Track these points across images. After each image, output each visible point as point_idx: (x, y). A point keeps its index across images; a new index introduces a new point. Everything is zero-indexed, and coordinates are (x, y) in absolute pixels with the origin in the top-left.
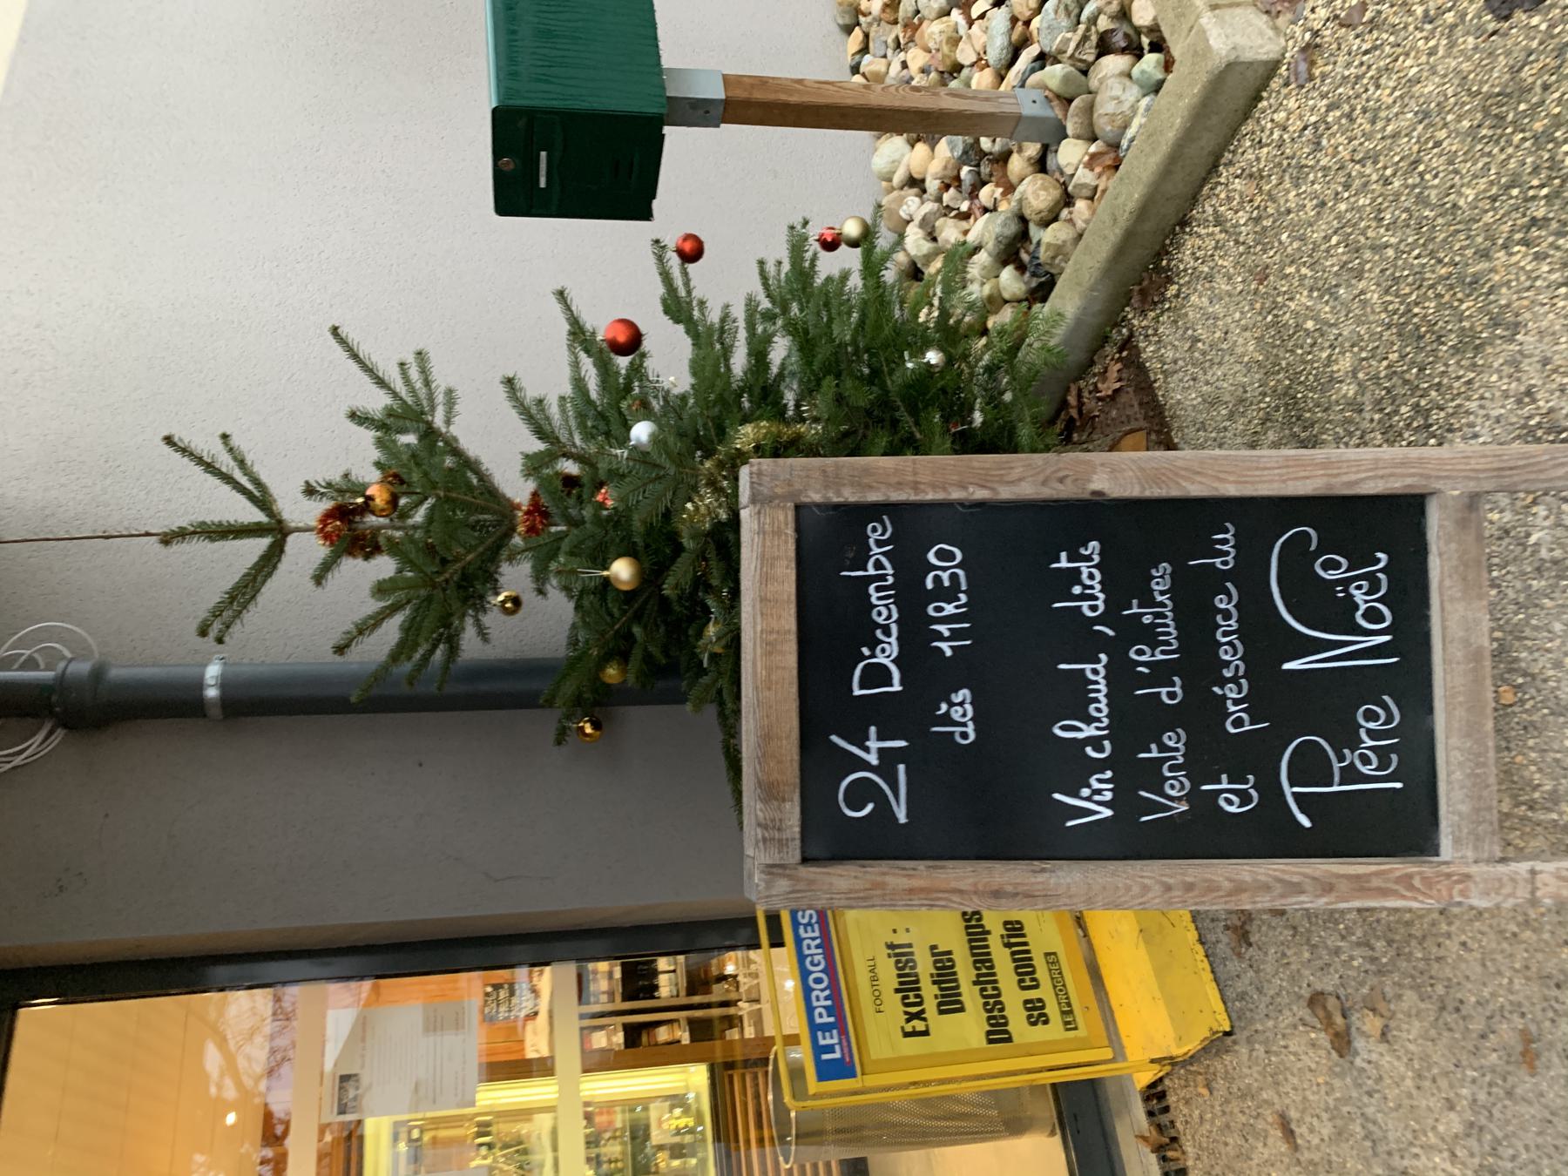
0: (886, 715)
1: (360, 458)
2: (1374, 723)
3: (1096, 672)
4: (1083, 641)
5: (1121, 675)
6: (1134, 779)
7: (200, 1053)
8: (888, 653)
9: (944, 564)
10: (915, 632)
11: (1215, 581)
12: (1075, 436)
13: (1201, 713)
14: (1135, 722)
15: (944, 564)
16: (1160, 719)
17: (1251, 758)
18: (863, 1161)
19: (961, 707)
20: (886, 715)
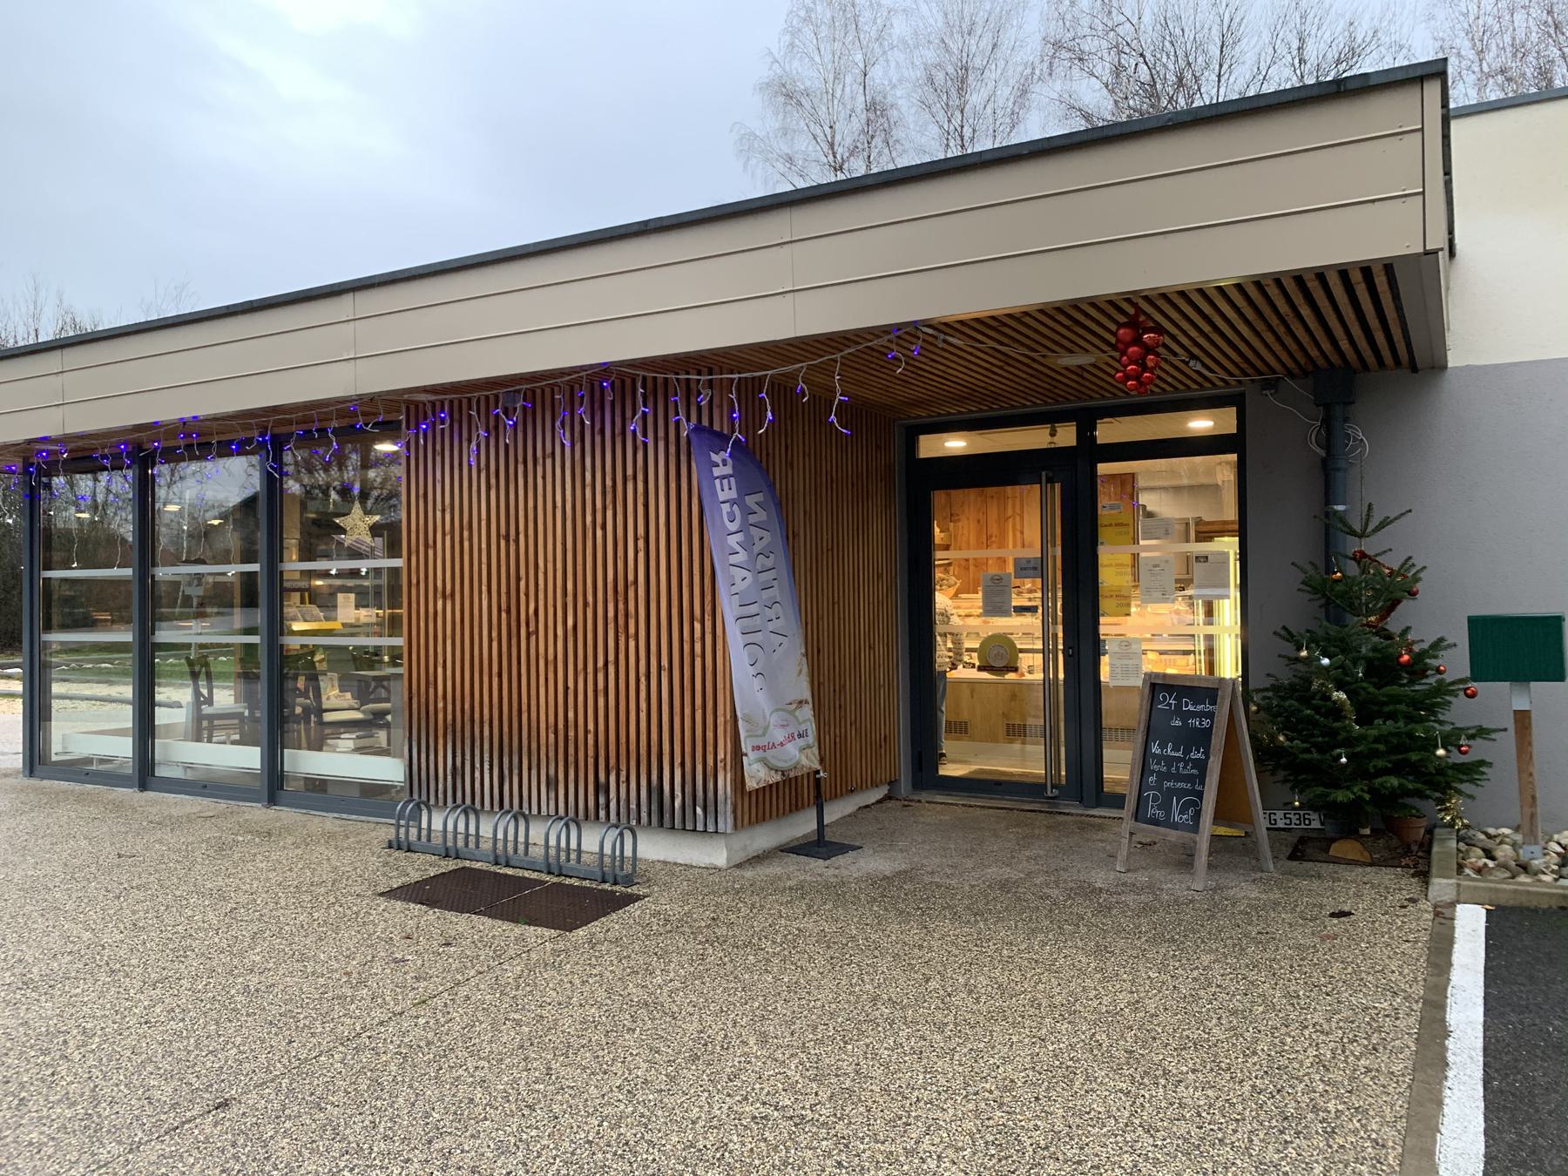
0: (1178, 706)
1: (1392, 562)
2: (1160, 814)
3: (1180, 754)
4: (1187, 751)
5: (1178, 759)
6: (1159, 758)
7: (1336, 512)
8: (1191, 708)
9: (1206, 723)
10: (1194, 715)
11: (1193, 785)
12: (384, 581)
13: (1167, 776)
14: (1170, 761)
15: (1206, 723)
16: (1169, 766)
17: (1159, 787)
18: (256, 606)
19: (1178, 723)
20: (1178, 706)
